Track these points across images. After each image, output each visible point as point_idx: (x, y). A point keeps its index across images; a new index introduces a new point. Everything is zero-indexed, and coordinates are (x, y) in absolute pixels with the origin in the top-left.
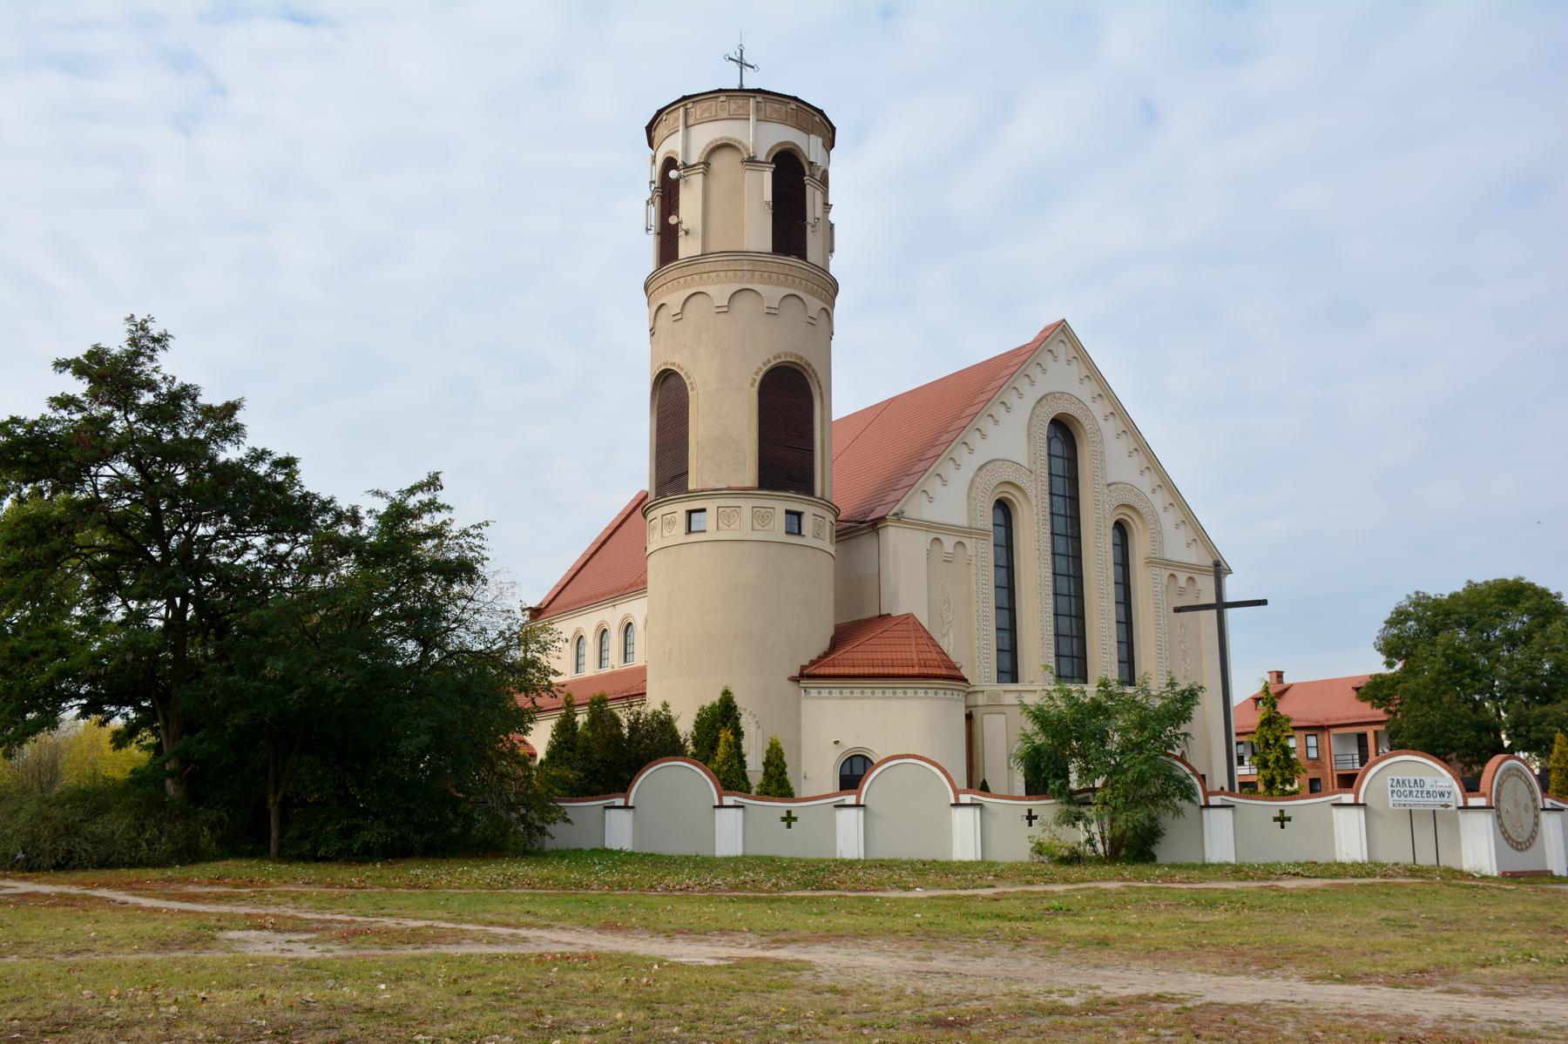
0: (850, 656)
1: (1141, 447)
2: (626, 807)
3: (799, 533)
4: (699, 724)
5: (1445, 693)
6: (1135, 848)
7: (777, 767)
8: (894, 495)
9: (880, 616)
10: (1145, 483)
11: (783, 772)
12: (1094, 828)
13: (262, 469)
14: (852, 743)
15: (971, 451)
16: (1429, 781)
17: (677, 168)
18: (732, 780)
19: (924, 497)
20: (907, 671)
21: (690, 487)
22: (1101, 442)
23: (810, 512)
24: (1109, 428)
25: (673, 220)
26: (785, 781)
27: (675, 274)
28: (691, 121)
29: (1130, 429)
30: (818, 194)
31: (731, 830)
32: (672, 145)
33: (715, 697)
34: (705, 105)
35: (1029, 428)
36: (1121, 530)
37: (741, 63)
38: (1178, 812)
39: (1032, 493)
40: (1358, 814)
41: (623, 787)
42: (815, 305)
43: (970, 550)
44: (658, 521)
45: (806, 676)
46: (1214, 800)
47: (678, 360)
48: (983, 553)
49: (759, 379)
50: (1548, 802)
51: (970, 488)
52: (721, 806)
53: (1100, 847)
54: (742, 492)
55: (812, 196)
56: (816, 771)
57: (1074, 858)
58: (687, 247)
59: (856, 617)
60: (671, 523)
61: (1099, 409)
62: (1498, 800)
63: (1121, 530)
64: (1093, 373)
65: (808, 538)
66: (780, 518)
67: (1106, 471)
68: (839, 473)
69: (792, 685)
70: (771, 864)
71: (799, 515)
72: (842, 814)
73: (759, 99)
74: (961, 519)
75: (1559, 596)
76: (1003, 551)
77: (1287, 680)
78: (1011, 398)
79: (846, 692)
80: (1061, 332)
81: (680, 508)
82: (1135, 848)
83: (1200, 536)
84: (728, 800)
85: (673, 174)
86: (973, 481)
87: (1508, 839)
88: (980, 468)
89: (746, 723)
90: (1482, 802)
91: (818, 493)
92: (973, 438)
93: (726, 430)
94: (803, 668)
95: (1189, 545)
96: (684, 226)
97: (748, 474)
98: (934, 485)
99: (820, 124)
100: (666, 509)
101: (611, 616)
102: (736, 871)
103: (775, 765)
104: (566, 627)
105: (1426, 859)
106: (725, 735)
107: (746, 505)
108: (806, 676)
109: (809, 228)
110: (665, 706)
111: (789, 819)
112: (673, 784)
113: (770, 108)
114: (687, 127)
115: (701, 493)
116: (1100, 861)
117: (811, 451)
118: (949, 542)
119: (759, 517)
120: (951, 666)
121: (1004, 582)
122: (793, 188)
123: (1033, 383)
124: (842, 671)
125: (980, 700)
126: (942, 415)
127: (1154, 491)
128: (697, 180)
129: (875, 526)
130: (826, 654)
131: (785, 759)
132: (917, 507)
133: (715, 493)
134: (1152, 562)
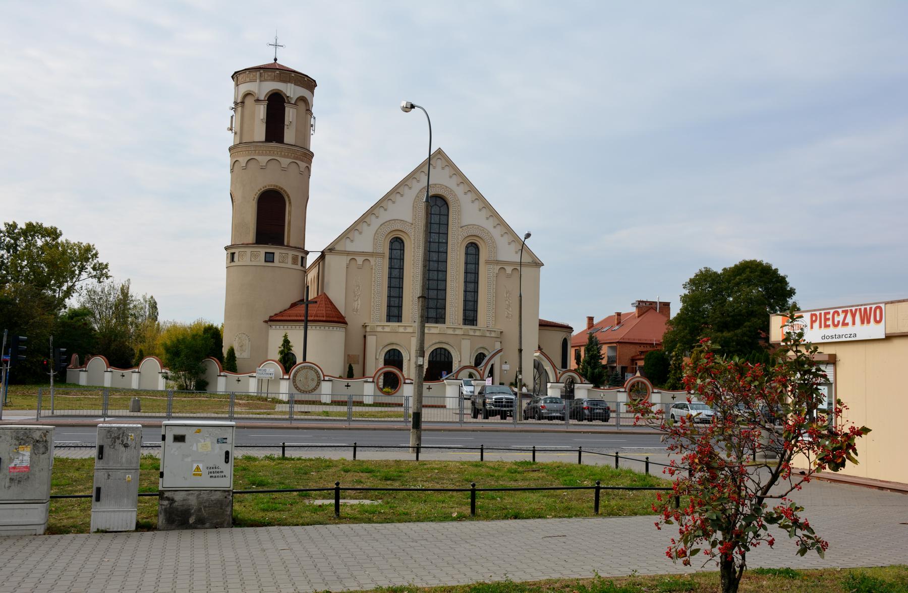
10: (489, 225)
36: (473, 250)
43: (372, 262)
54: (247, 245)
61: (459, 191)
63: (473, 250)
64: (457, 172)
65: (276, 263)
67: (464, 220)
74: (369, 249)
75: (776, 270)
113: (266, 75)
117: (284, 226)
118: (360, 260)
119: (254, 256)
127: (495, 227)
134: (488, 262)
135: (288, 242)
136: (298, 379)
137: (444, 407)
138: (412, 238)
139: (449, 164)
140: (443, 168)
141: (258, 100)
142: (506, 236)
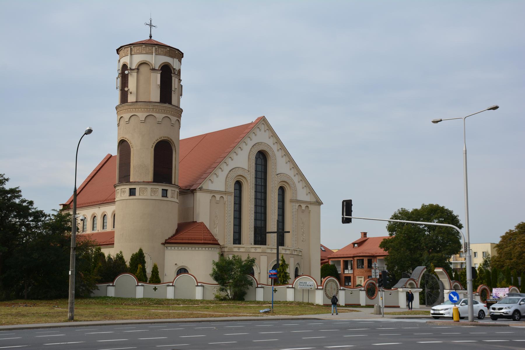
0: (181, 236)
1: (291, 160)
2: (113, 286)
3: (166, 196)
4: (132, 259)
5: (402, 247)
6: (240, 296)
7: (156, 273)
8: (200, 181)
9: (193, 222)
11: (158, 274)
12: (229, 292)
13: (25, 204)
14: (181, 264)
15: (227, 165)
16: (308, 282)
17: (127, 70)
18: (142, 278)
19: (210, 182)
20: (200, 242)
21: (131, 181)
22: (276, 159)
23: (170, 189)
24: (279, 154)
25: (126, 89)
26: (158, 277)
27: (127, 107)
28: (133, 53)
29: (287, 154)
30: (177, 80)
31: (140, 292)
32: (126, 60)
33: (137, 251)
34: (138, 48)
35: (249, 156)
36: (282, 190)
37: (151, 25)
38: (248, 288)
39: (248, 179)
40: (293, 290)
41: (113, 281)
42: (174, 119)
43: (225, 199)
44: (120, 191)
45: (168, 243)
46: (259, 286)
47: (127, 137)
48: (230, 200)
49: (154, 145)
50: (342, 288)
51: (226, 178)
52: (138, 286)
53: (230, 297)
54: (148, 183)
55: (175, 80)
56: (168, 273)
57: (224, 299)
58: (131, 98)
59: (186, 221)
60: (124, 192)
61: (275, 148)
62: (325, 287)
63: (282, 190)
64: (274, 135)
65: (169, 198)
66: (160, 192)
67: (278, 168)
68: (181, 173)
69: (162, 246)
70: (149, 300)
71: (167, 190)
72: (169, 288)
73: (157, 47)
74: (223, 189)
76: (237, 199)
77: (368, 236)
78: (243, 146)
79: (180, 248)
80: (263, 120)
81: (127, 188)
82: (240, 296)
83: (312, 191)
84: (140, 284)
85: (126, 72)
86: (227, 175)
87: (327, 295)
88: (230, 171)
89: (147, 259)
90: (321, 287)
91: (173, 183)
92: (229, 161)
93: (142, 161)
94: (166, 240)
95: (307, 195)
96: (130, 91)
97: (150, 177)
98: (213, 178)
99: (178, 55)
100: (122, 187)
101: (98, 211)
102: (141, 301)
103: (155, 271)
104: (81, 214)
105: (306, 301)
106: (140, 266)
107: (149, 187)
108: (168, 243)
109: (173, 92)
110: (121, 252)
111: (155, 289)
112: (126, 280)
114: (131, 54)
115: (134, 183)
116: (230, 299)
118: (218, 197)
119: (154, 192)
120: (216, 240)
121: (238, 209)
122: (168, 77)
123: (251, 140)
124: (177, 241)
125: (226, 250)
126: (226, 141)
127: (295, 176)
128: (135, 74)
129: (193, 191)
130: (174, 235)
131: (159, 270)
132: (208, 185)
133: (138, 183)
134: (292, 201)
135: (175, 182)
136: (327, 289)
137: (399, 307)
138: (249, 182)
139: (270, 128)
140: (265, 131)
141: (153, 69)
142: (301, 182)
